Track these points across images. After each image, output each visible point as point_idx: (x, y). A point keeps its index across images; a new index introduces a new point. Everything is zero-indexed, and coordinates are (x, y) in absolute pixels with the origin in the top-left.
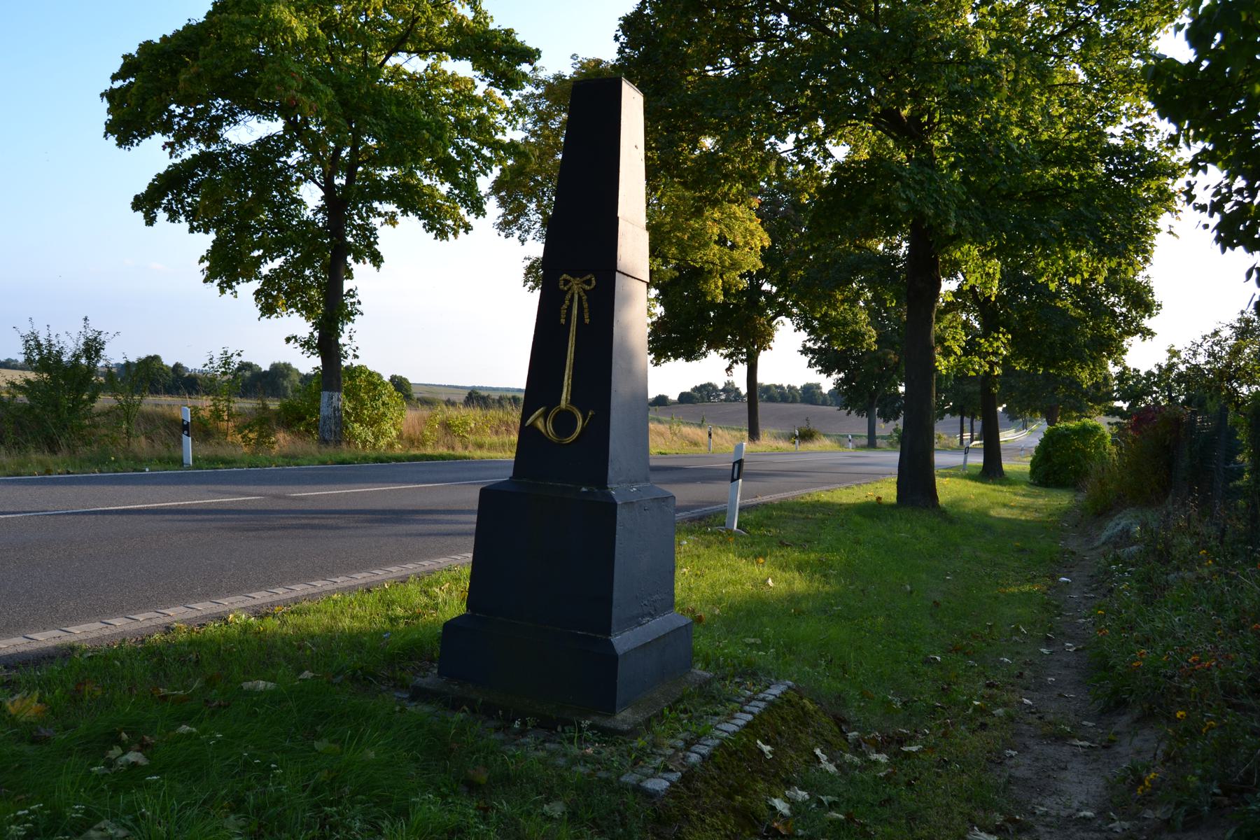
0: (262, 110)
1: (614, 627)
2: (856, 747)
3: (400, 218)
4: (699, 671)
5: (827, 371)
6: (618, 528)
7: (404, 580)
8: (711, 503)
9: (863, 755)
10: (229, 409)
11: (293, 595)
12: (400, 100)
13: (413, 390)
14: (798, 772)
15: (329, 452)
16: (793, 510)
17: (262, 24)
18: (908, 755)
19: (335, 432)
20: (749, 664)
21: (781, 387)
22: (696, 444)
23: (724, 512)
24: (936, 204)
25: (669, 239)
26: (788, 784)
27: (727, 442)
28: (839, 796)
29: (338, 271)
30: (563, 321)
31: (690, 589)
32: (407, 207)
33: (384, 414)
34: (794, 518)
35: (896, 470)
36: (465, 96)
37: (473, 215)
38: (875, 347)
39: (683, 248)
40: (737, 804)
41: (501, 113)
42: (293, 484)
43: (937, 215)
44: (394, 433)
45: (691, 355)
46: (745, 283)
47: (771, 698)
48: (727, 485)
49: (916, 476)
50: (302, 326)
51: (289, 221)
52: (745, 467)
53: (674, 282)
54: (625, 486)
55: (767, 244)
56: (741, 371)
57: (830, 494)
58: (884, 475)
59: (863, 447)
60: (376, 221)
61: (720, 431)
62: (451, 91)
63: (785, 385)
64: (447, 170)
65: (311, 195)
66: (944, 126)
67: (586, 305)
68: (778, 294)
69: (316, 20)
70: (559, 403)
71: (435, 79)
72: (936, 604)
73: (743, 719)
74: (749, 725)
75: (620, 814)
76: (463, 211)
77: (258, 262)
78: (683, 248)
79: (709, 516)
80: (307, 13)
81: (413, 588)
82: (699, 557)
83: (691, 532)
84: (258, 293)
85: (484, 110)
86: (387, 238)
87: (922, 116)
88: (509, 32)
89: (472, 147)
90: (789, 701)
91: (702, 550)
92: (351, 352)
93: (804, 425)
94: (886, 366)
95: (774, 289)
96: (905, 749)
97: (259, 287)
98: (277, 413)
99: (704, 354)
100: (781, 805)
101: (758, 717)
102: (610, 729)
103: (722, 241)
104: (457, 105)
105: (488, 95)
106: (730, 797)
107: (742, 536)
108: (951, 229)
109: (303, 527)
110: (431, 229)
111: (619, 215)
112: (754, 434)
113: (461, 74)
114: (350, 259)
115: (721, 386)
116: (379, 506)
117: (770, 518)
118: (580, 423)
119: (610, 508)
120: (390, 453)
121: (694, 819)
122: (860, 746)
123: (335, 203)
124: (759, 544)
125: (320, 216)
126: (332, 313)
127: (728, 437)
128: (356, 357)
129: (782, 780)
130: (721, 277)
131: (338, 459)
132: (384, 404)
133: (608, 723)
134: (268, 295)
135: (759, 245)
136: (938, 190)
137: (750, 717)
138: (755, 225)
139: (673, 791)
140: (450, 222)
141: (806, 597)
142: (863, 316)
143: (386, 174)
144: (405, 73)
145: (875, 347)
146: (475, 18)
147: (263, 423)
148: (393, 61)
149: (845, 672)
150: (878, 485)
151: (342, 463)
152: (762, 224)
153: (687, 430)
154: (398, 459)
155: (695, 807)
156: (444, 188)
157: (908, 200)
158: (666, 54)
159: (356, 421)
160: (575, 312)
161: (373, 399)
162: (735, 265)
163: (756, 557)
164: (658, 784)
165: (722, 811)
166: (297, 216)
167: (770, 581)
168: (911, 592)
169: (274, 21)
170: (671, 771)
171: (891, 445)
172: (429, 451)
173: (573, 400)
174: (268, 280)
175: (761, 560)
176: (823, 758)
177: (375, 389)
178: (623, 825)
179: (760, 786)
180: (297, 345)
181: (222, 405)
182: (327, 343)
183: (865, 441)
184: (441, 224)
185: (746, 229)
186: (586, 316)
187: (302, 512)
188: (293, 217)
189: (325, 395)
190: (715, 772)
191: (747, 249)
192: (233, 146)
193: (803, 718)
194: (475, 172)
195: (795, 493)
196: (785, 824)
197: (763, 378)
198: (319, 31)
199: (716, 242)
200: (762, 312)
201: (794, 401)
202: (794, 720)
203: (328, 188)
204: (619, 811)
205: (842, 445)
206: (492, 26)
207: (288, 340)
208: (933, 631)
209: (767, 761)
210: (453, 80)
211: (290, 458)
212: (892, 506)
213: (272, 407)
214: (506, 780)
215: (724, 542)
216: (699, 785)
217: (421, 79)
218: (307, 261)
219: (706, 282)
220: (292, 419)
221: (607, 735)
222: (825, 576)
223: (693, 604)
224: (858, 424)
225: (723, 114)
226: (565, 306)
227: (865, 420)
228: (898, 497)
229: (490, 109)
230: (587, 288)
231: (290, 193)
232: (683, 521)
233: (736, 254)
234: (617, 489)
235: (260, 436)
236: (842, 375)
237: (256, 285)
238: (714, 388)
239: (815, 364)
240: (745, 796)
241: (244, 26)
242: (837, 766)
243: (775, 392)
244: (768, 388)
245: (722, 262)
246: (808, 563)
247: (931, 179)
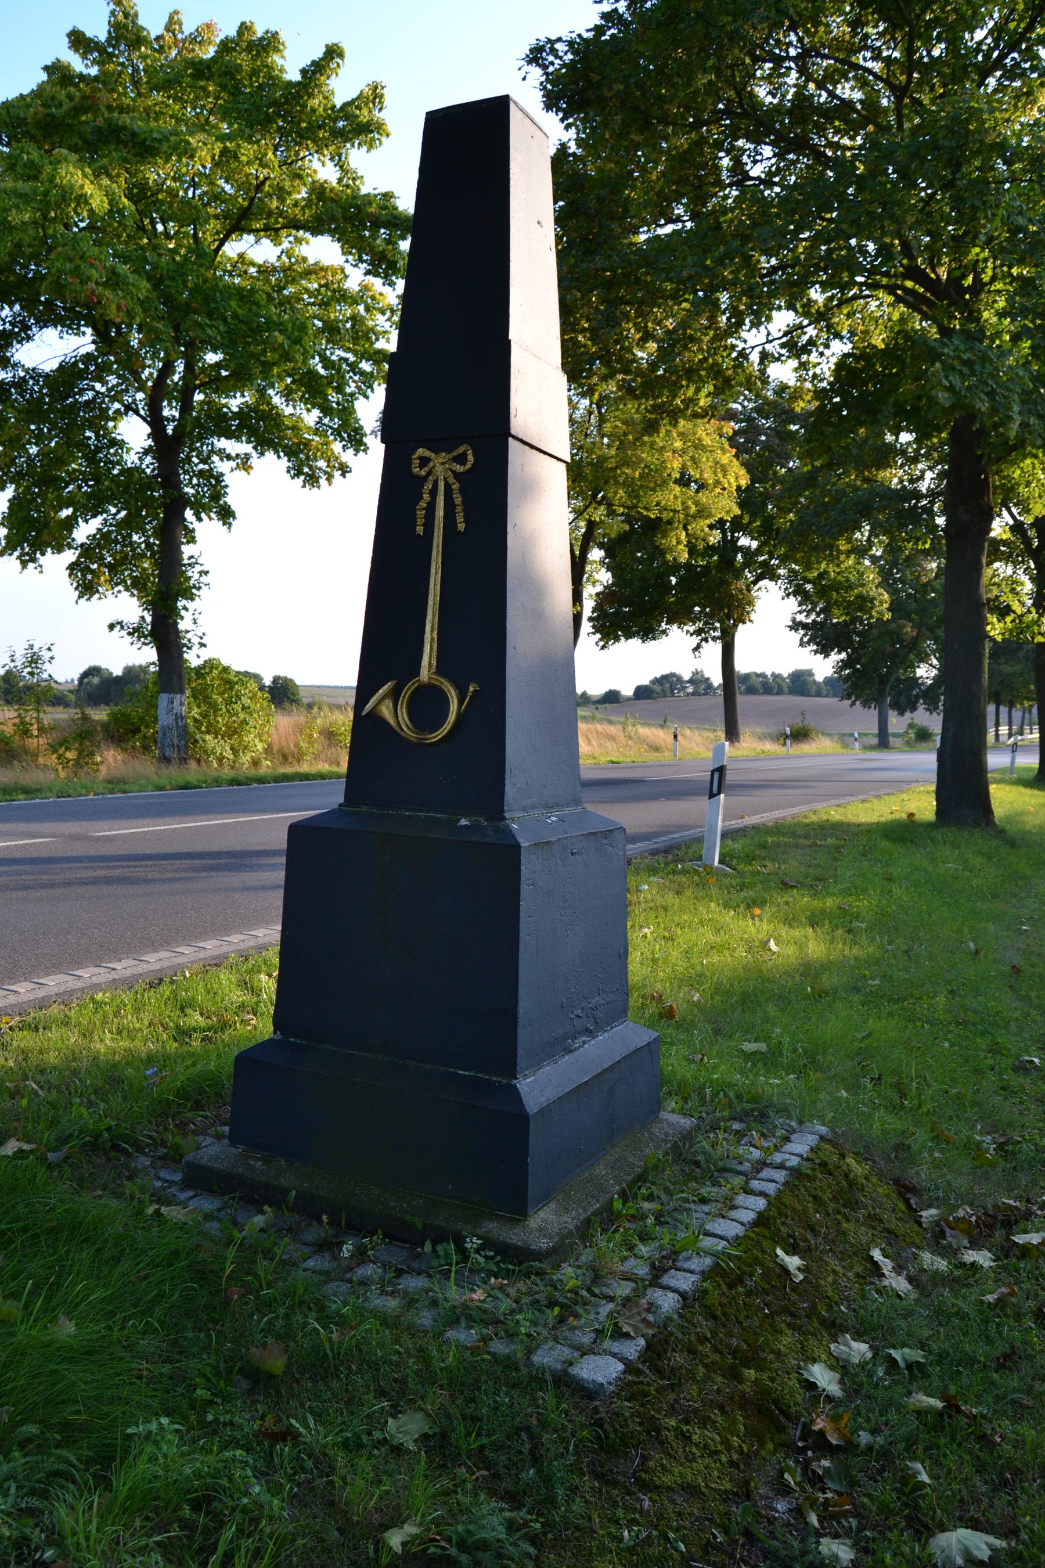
0: (69, 322)
1: (521, 1063)
2: (936, 1238)
3: (255, 461)
4: (674, 1118)
5: (824, 650)
6: (524, 888)
7: (217, 963)
8: (681, 828)
9: (950, 1253)
10: (39, 720)
11: (40, 993)
12: (245, 296)
13: (302, 694)
14: (847, 1299)
15: (173, 773)
16: (794, 835)
17: (46, 194)
18: (1025, 1251)
19: (182, 746)
20: (755, 1099)
21: (763, 675)
22: (657, 749)
23: (699, 840)
24: (991, 394)
25: (615, 478)
26: (835, 1328)
27: (697, 746)
28: (922, 1346)
29: (172, 534)
30: (420, 530)
31: (654, 960)
32: (263, 444)
33: (244, 722)
34: (797, 846)
35: (934, 777)
36: (334, 291)
37: (351, 451)
38: (888, 616)
39: (634, 491)
40: (746, 1387)
41: (383, 313)
42: (100, 819)
43: (994, 410)
44: (260, 746)
45: (648, 632)
46: (715, 537)
47: (794, 1161)
48: (703, 802)
49: (962, 784)
50: (128, 607)
51: (109, 471)
52: (730, 777)
53: (623, 538)
54: (537, 813)
55: (744, 482)
56: (713, 650)
57: (841, 810)
58: (909, 782)
59: (872, 748)
60: (222, 466)
61: (688, 732)
62: (316, 286)
63: (769, 673)
64: (311, 388)
65: (134, 433)
66: (999, 286)
67: (458, 499)
68: (759, 551)
69: (119, 187)
70: (418, 674)
71: (293, 271)
72: (1016, 970)
73: (750, 1207)
74: (762, 1220)
75: (531, 1437)
76: (337, 447)
77: (70, 524)
78: (634, 491)
79: (678, 847)
80: (108, 175)
81: (226, 979)
82: (665, 909)
83: (653, 871)
84: (72, 567)
85: (361, 308)
86: (238, 488)
87: (964, 276)
88: (388, 196)
89: (346, 360)
90: (823, 1164)
91: (671, 898)
92: (195, 640)
93: (798, 722)
94: (901, 641)
95: (755, 544)
96: (1019, 1239)
97: (73, 559)
98: (105, 726)
99: (664, 632)
100: (822, 1376)
101: (775, 1202)
102: (516, 1248)
103: (684, 481)
104: (325, 304)
105: (365, 288)
106: (734, 1375)
107: (726, 875)
108: (1013, 430)
109: (95, 881)
110: (299, 473)
111: (511, 337)
112: (732, 733)
113: (326, 262)
114: (189, 514)
115: (687, 677)
116: (214, 847)
117: (764, 846)
118: (454, 706)
119: (507, 856)
120: (253, 772)
121: (671, 1436)
122: (942, 1234)
123: (166, 447)
124: (752, 886)
125: (148, 459)
126: (166, 590)
127: (698, 739)
128: (202, 645)
129: (823, 1322)
130: (685, 528)
131: (181, 781)
132: (244, 708)
133: (513, 1236)
134: (87, 570)
135: (734, 485)
136: (995, 377)
137: (761, 1203)
138: (727, 457)
139: (630, 1384)
140: (322, 464)
141: (826, 966)
142: (871, 576)
143: (235, 403)
144: (253, 264)
145: (888, 616)
146: (340, 180)
147: (83, 738)
148: (232, 249)
149: (903, 1095)
150: (904, 796)
151: (185, 787)
152: (736, 456)
153: (644, 731)
154: (261, 780)
155: (672, 1412)
156: (311, 417)
157: (951, 389)
158: (600, 200)
159: (208, 732)
160: (440, 512)
161: (229, 702)
162: (702, 512)
163: (748, 907)
164: (601, 1370)
165: (722, 1408)
166: (119, 463)
167: (772, 944)
168: (977, 952)
169: (62, 187)
170: (627, 1336)
171: (908, 743)
172: (305, 768)
173: (442, 668)
174: (86, 551)
175: (757, 911)
176: (887, 1265)
177: (231, 688)
178: (536, 1460)
179: (787, 1340)
180: (124, 633)
181: (30, 716)
182: (164, 632)
183: (875, 741)
184: (310, 467)
185: (717, 463)
186: (460, 518)
187: (103, 859)
188: (114, 464)
189: (163, 698)
190: (705, 1326)
191: (718, 490)
192: (27, 371)
193: (849, 1194)
194: (352, 395)
195: (795, 810)
196: (835, 1419)
197: (742, 665)
198: (125, 200)
199: (676, 482)
200: (738, 574)
201: (780, 692)
202: (834, 1199)
203: (155, 421)
204: (528, 1429)
205: (846, 746)
206: (364, 190)
207: (111, 627)
208: (1017, 1014)
209: (795, 1287)
210: (316, 270)
211: (116, 783)
212: (930, 825)
213: (96, 717)
214: (320, 1367)
215: (702, 885)
216: (678, 1359)
217: (274, 269)
218: (130, 524)
219: (665, 535)
220: (122, 732)
221: (515, 1259)
222: (849, 931)
223: (659, 987)
224: (864, 719)
225: (685, 274)
226: (423, 504)
227: (873, 713)
228: (939, 812)
229: (367, 309)
230: (459, 468)
231: (108, 432)
232: (642, 855)
233: (703, 497)
234: (524, 817)
235: (80, 752)
236: (843, 655)
237: (70, 556)
238: (679, 679)
239: (808, 643)
240: (760, 1369)
241: (21, 196)
242: (911, 1280)
243: (757, 682)
244: (747, 677)
245: (686, 508)
246: (823, 912)
247: (984, 358)
